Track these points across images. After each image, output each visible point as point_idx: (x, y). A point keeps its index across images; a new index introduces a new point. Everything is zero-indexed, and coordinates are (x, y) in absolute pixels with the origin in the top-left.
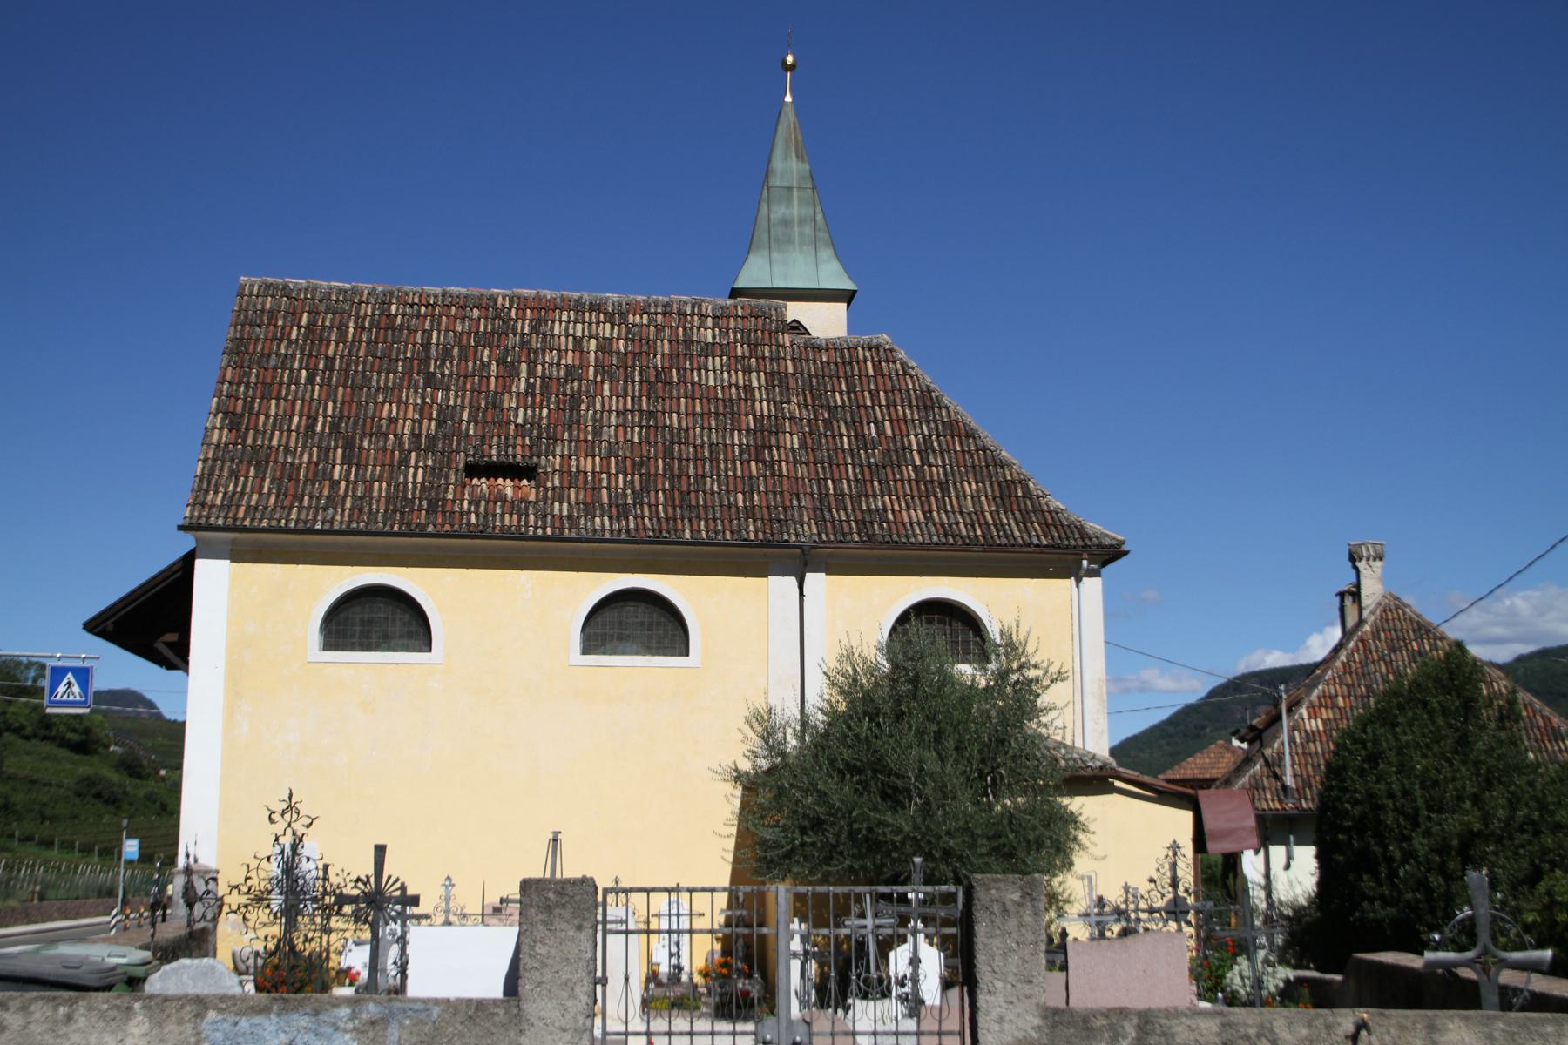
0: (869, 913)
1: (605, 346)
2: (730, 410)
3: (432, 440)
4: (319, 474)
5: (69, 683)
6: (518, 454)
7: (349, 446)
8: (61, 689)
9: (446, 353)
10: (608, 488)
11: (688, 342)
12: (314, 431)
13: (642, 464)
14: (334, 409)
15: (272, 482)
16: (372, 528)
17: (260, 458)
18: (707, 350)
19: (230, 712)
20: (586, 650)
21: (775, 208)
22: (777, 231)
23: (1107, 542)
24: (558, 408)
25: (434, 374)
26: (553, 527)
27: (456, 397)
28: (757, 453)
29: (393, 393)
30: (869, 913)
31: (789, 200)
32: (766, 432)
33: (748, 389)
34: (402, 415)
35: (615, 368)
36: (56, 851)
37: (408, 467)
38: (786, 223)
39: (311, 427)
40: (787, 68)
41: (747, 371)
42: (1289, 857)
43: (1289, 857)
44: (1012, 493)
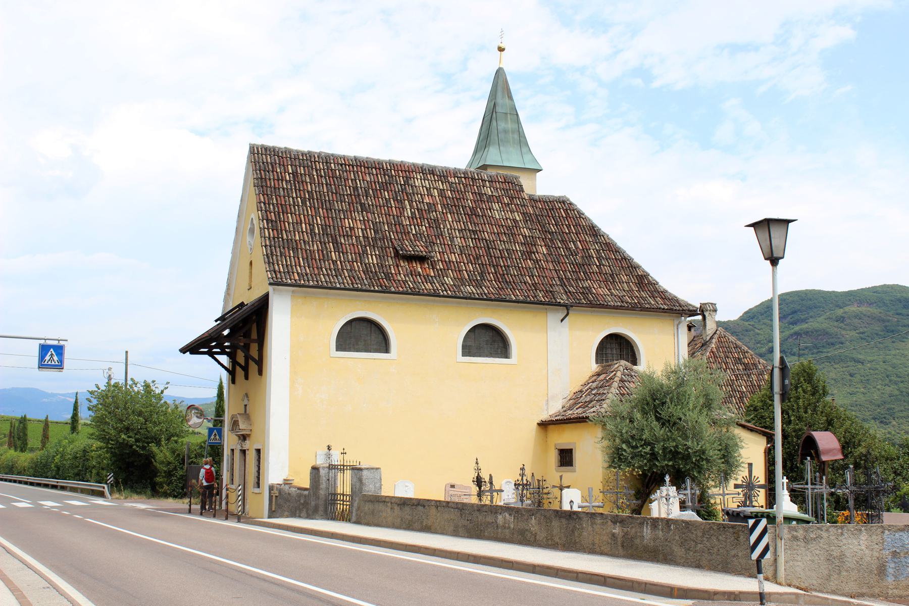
0: (689, 488)
1: (442, 193)
2: (511, 231)
3: (375, 239)
4: (325, 258)
5: (52, 355)
6: (420, 248)
7: (335, 242)
8: (48, 358)
11: (481, 194)
15: (303, 259)
16: (364, 288)
18: (490, 198)
21: (499, 123)
22: (501, 136)
23: (691, 308)
28: (529, 254)
29: (348, 213)
30: (689, 488)
31: (506, 120)
32: (530, 243)
33: (515, 220)
34: (355, 223)
35: (453, 206)
38: (506, 131)
39: (312, 230)
41: (512, 212)
42: (329, 456)
43: (329, 456)
44: (643, 281)
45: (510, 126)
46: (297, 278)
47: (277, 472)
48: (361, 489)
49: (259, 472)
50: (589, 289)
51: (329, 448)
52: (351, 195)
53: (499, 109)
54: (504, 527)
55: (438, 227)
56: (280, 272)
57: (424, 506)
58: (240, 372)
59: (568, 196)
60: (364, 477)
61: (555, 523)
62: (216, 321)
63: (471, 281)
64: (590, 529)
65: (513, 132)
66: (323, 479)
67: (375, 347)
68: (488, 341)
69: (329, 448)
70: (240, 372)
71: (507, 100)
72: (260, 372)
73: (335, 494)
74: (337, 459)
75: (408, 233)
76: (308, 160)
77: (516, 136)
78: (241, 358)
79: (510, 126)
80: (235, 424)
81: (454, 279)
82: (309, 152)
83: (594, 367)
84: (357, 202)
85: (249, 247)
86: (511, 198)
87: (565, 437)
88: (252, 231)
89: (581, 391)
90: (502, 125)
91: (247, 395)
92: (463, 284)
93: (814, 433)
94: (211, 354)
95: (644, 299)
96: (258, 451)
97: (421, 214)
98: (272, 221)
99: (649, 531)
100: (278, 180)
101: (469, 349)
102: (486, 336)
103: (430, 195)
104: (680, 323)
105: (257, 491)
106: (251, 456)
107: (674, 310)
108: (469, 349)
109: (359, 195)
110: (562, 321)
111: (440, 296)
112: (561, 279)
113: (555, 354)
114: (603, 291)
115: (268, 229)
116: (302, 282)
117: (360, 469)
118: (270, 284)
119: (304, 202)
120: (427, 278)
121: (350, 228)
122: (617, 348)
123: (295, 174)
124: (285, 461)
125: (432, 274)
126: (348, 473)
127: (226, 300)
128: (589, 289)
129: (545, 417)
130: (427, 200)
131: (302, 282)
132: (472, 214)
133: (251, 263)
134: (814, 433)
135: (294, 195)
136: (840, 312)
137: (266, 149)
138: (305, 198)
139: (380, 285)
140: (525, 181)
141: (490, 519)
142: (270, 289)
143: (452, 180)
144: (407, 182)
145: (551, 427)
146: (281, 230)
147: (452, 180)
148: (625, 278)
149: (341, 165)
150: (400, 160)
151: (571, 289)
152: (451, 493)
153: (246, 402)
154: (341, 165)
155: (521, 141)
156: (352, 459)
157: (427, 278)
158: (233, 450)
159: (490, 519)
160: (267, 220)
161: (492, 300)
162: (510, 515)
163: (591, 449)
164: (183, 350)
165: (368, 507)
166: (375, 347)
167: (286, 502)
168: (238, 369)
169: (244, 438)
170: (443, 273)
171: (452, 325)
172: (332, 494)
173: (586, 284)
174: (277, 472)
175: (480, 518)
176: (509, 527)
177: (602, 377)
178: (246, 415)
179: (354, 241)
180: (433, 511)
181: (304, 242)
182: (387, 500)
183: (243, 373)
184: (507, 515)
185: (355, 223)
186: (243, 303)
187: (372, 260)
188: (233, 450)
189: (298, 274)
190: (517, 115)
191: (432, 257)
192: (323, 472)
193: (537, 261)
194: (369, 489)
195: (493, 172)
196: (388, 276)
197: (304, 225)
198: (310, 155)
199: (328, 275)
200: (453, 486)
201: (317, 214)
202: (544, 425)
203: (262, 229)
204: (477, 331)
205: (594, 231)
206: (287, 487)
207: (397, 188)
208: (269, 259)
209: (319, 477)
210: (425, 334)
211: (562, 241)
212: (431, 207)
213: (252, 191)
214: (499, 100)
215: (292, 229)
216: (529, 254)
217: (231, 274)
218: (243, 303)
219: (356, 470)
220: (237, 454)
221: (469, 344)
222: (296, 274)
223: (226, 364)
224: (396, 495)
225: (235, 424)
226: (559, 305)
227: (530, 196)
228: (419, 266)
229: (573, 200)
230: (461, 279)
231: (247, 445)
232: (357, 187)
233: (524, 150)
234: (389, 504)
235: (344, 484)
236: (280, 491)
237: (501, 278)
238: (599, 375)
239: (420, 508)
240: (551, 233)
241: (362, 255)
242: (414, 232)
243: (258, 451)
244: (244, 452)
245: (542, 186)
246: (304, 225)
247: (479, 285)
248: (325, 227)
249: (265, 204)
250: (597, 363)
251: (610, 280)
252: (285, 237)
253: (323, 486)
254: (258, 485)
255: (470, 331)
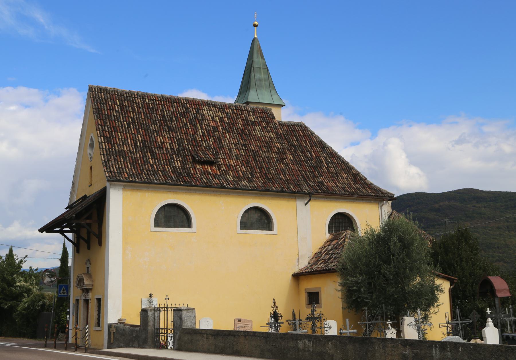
1: (221, 119)
2: (269, 145)
3: (178, 150)
6: (210, 156)
7: (152, 152)
9: (171, 120)
10: (241, 171)
11: (247, 121)
12: (137, 146)
13: (248, 163)
14: (141, 137)
17: (122, 154)
18: (254, 123)
19: (124, 249)
20: (241, 229)
21: (256, 74)
22: (258, 83)
24: (215, 142)
25: (170, 126)
26: (138, 178)
27: (180, 136)
29: (159, 133)
31: (260, 72)
33: (271, 138)
34: (164, 139)
35: (230, 128)
36: (380, 321)
37: (174, 160)
38: (260, 80)
39: (136, 144)
40: (255, 26)
43: (151, 302)
45: (263, 76)
46: (127, 176)
47: (113, 316)
48: (181, 325)
49: (99, 315)
50: (322, 183)
51: (151, 296)
52: (161, 120)
53: (255, 65)
54: (304, 350)
55: (220, 141)
56: (114, 172)
57: (234, 336)
58: (83, 244)
59: (304, 122)
60: (184, 316)
61: (350, 347)
62: (66, 209)
63: (245, 178)
64: (382, 351)
65: (265, 80)
66: (151, 319)
67: (181, 224)
68: (258, 220)
69: (151, 296)
70: (83, 244)
71: (260, 59)
72: (100, 244)
73: (160, 329)
74: (157, 302)
75: (201, 146)
76: (129, 97)
77: (267, 83)
78: (84, 233)
79: (263, 76)
80: (80, 281)
81: (233, 177)
82: (130, 91)
83: (327, 236)
84: (164, 124)
85: (89, 157)
86: (268, 123)
87: (312, 284)
88: (92, 146)
89: (320, 252)
90: (258, 76)
91: (89, 260)
92: (240, 180)
93: (489, 277)
94: (62, 232)
95: (359, 189)
96: (99, 300)
97: (209, 133)
98: (107, 137)
99: (438, 352)
100: (110, 110)
101: (245, 225)
102: (256, 215)
103: (213, 120)
104: (382, 205)
105: (98, 328)
106: (93, 305)
107: (377, 196)
108: (245, 225)
109: (166, 121)
110: (306, 204)
111: (225, 188)
112: (303, 177)
113: (303, 227)
114: (332, 184)
115: (105, 143)
116: (131, 179)
117: (180, 310)
118: (108, 181)
119: (129, 125)
120: (215, 176)
121: (161, 142)
122: (341, 223)
123: (121, 105)
124: (120, 307)
125: (219, 173)
126: (171, 314)
127: (71, 194)
128: (322, 183)
129: (296, 270)
130: (212, 124)
131: (131, 179)
132: (242, 133)
133: (91, 168)
134: (489, 277)
135: (122, 120)
136: (437, 206)
137: (101, 89)
138: (129, 122)
139: (186, 182)
140: (275, 111)
141: (291, 344)
142: (108, 184)
143: (228, 111)
144: (197, 112)
145: (301, 277)
146: (114, 144)
147: (228, 111)
148: (345, 176)
149: (153, 100)
150: (192, 97)
151: (310, 183)
152: (239, 325)
153: (88, 265)
154: (153, 100)
155: (271, 87)
156: (176, 301)
157: (215, 176)
158: (77, 300)
159: (291, 344)
160: (104, 137)
161: (260, 191)
162: (309, 341)
163: (331, 291)
164: (41, 230)
165: (186, 338)
166: (181, 224)
167: (121, 335)
168: (82, 241)
169: (87, 291)
170: (227, 173)
171: (239, 205)
172: (157, 329)
173: (320, 179)
174: (113, 316)
175: (283, 343)
176: (309, 351)
177: (334, 242)
178: (88, 274)
179: (165, 151)
180: (242, 340)
181: (130, 151)
182: (203, 332)
183: (86, 245)
184: (307, 341)
185: (164, 139)
186: (86, 195)
187: (178, 164)
188: (77, 300)
189: (127, 173)
190: (267, 69)
191: (218, 162)
192: (150, 313)
193: (287, 165)
194: (187, 325)
195: (254, 106)
196: (189, 174)
197: (129, 141)
198: (131, 94)
199: (148, 174)
200: (239, 321)
201: (138, 132)
202: (297, 277)
203: (100, 144)
204: (249, 212)
205: (322, 145)
206: (122, 325)
207: (192, 116)
208: (106, 164)
209: (148, 316)
210: (216, 213)
211: (302, 152)
212: (216, 129)
213: (92, 117)
214: (255, 59)
215: (121, 143)
216: (281, 160)
217: (75, 176)
218: (86, 195)
219: (177, 311)
220: (81, 304)
221: (245, 221)
222: (126, 174)
223: (72, 239)
224: (253, 331)
225: (80, 281)
226: (304, 193)
227: (279, 122)
228: (209, 168)
229: (307, 124)
230: (239, 177)
231: (90, 295)
232: (164, 115)
233: (273, 92)
234: (205, 335)
235: (166, 321)
236: (117, 328)
237: (264, 176)
238: (331, 241)
239: (231, 338)
240: (295, 146)
241: (170, 162)
242: (205, 145)
243: (99, 300)
244: (87, 301)
245: (284, 116)
246: (129, 141)
247: (250, 181)
248: (144, 142)
249: (101, 126)
250: (329, 233)
251: (335, 177)
252: (117, 148)
253: (151, 323)
254: (99, 324)
255: (245, 212)
